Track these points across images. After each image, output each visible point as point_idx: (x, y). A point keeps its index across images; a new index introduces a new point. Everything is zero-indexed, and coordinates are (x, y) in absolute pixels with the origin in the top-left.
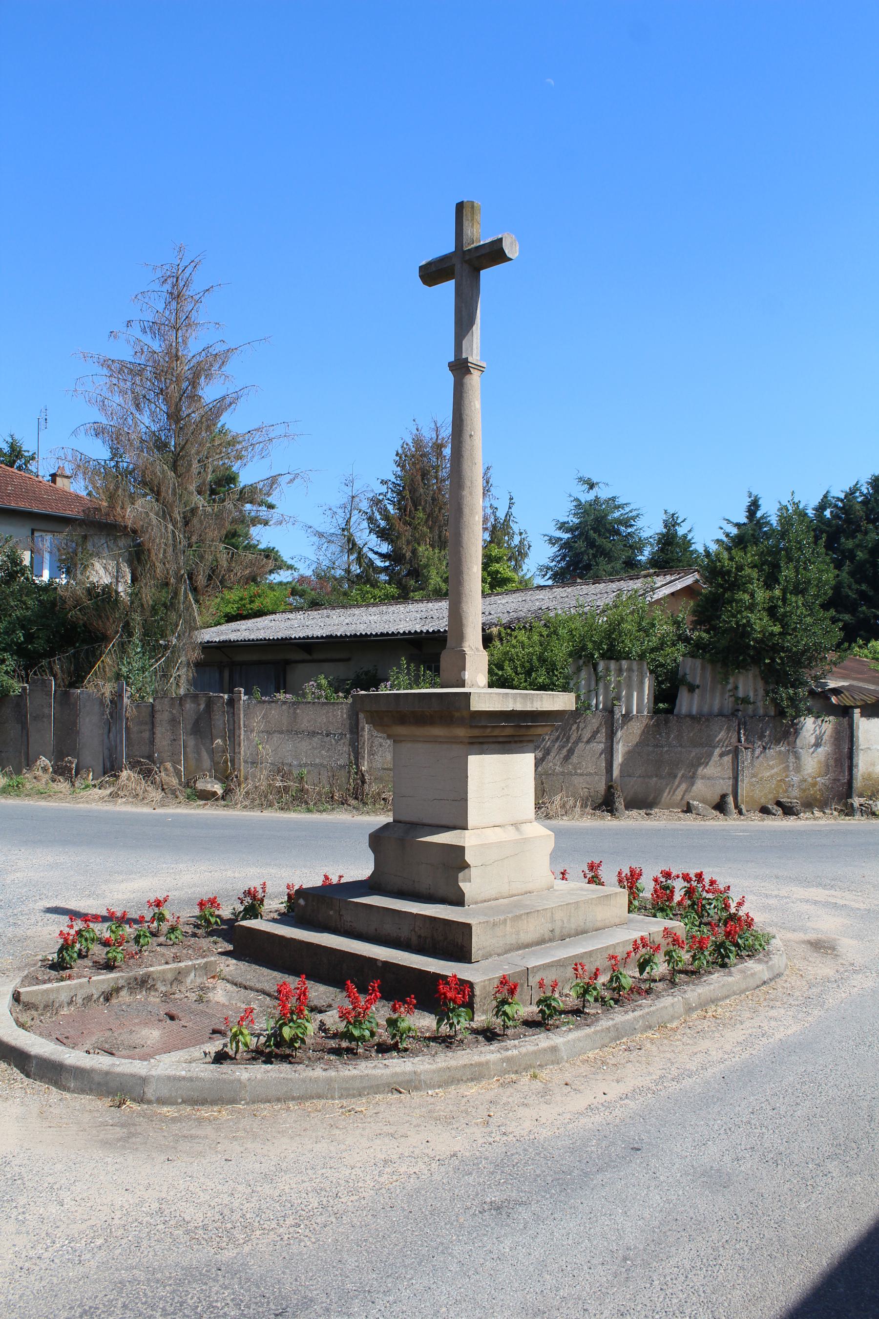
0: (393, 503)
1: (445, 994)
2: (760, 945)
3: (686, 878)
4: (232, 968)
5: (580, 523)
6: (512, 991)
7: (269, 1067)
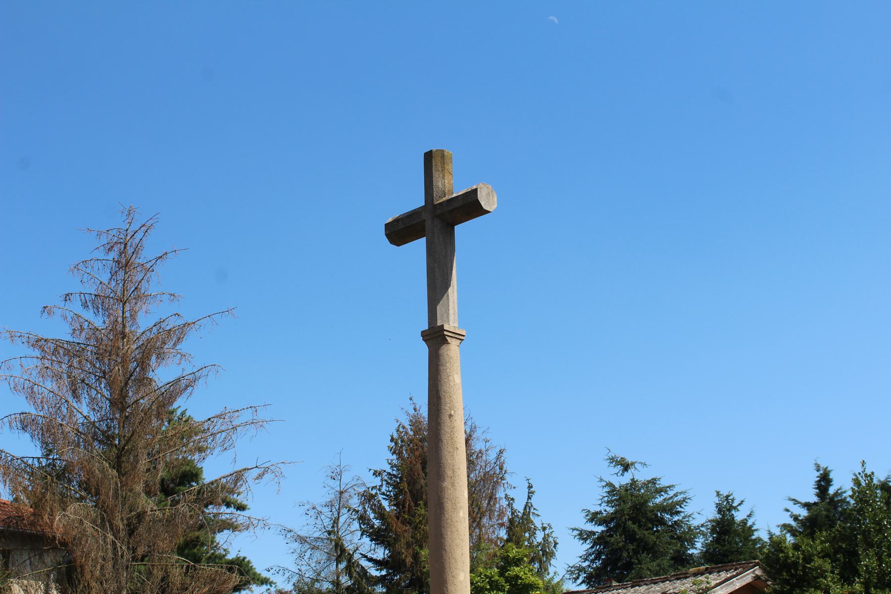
5: (616, 512)
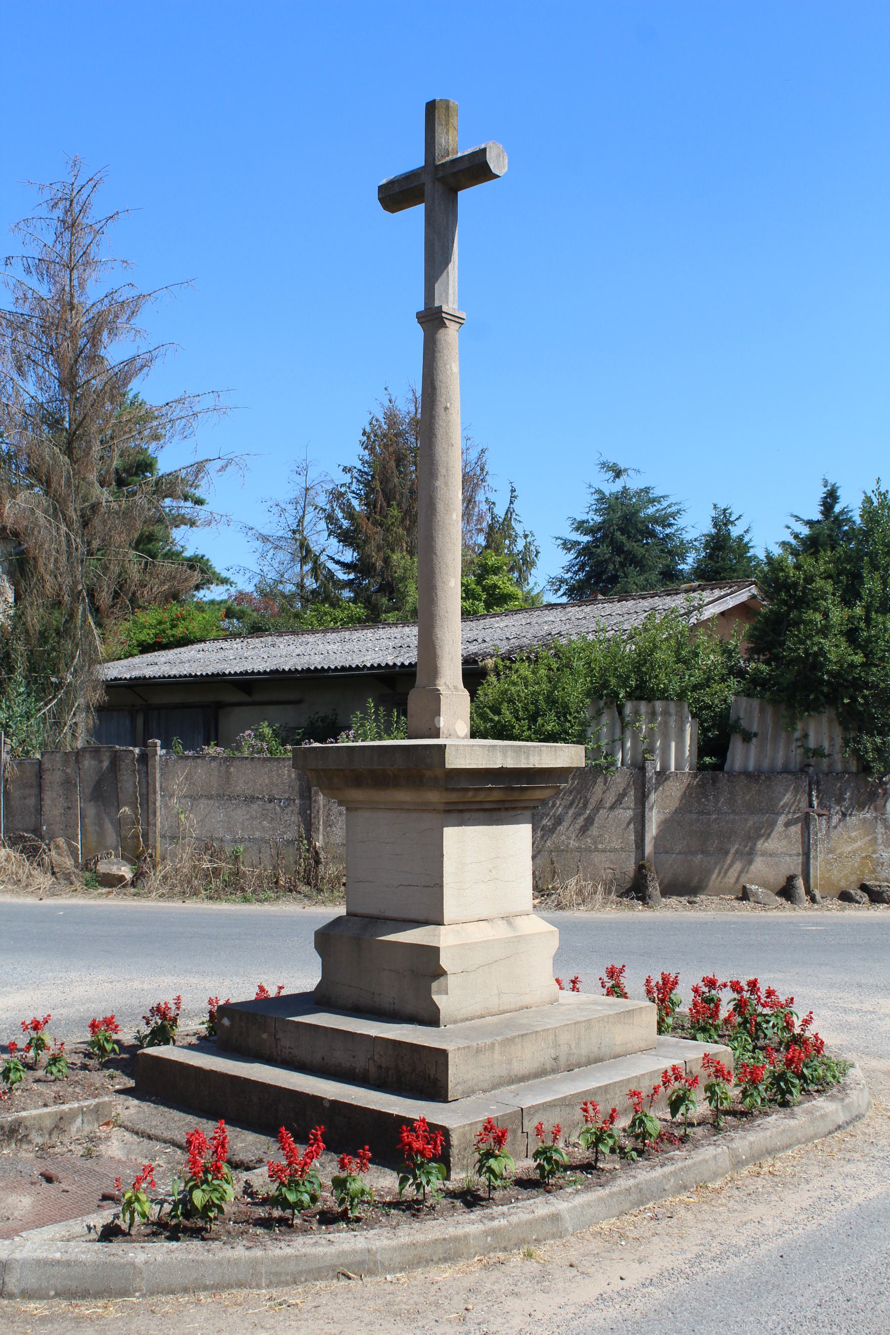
0: (358, 496)
1: (410, 1144)
2: (834, 1077)
3: (736, 987)
4: (132, 1110)
5: (604, 522)
6: (500, 1140)
7: (175, 1244)
